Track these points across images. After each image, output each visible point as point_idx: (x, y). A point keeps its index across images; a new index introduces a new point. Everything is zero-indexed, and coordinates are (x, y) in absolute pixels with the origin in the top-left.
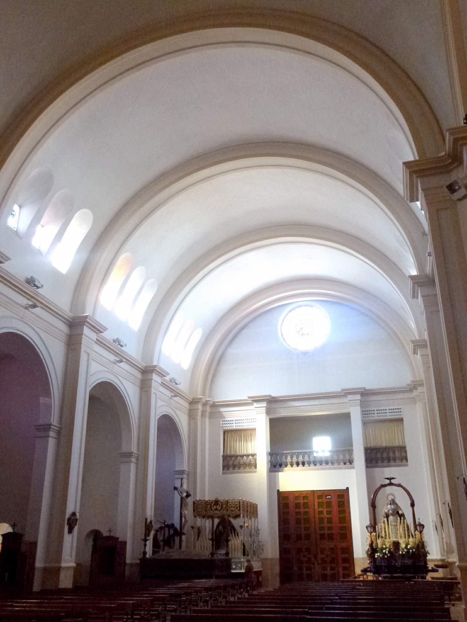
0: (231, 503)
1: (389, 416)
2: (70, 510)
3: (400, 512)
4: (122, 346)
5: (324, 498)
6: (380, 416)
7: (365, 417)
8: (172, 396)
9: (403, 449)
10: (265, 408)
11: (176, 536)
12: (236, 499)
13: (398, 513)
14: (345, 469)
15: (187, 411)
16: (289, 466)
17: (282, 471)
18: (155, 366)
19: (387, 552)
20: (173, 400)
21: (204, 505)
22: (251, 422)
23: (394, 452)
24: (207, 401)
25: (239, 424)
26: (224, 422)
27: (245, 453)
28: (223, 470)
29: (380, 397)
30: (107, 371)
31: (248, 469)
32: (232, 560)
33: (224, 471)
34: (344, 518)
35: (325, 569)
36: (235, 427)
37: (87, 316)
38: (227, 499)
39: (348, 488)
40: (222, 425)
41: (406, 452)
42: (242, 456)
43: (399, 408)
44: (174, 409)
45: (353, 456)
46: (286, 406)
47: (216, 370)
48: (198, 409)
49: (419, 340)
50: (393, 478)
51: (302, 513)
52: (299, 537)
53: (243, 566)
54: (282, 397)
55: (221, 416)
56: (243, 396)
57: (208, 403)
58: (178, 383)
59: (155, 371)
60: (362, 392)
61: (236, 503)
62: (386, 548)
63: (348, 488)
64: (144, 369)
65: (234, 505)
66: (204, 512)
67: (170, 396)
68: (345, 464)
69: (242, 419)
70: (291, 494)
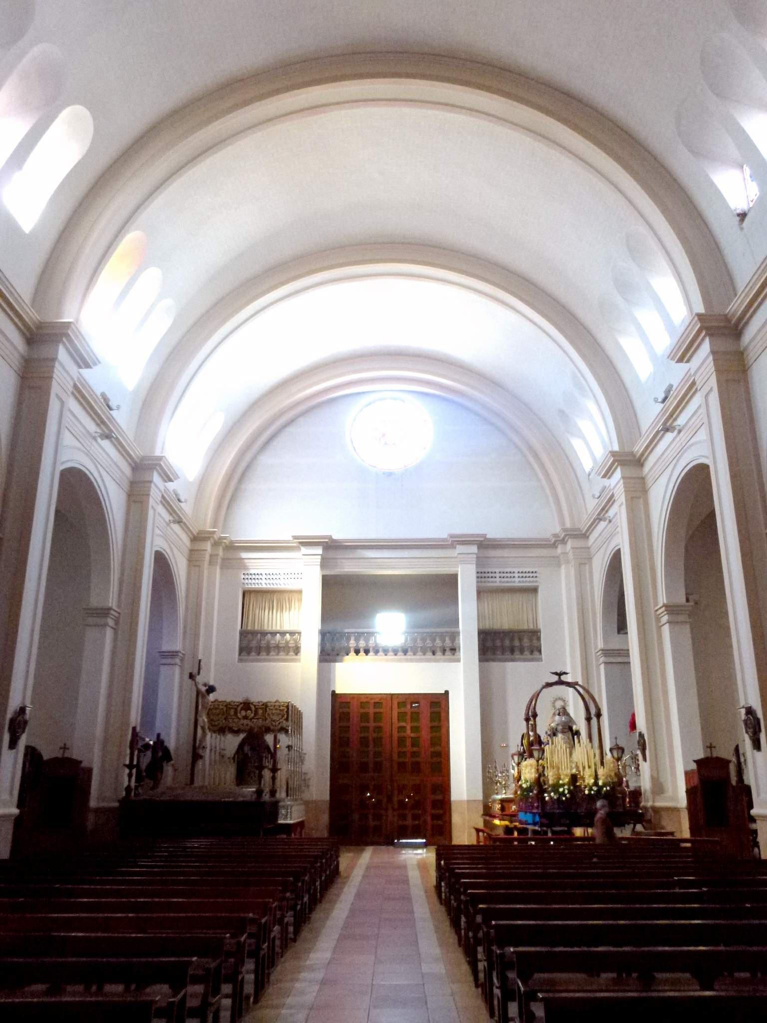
1: (517, 582)
2: (14, 703)
3: (574, 728)
4: (111, 409)
5: (409, 707)
6: (504, 582)
7: (481, 582)
8: (170, 521)
9: (535, 634)
11: (165, 762)
12: (281, 700)
13: (571, 729)
14: (445, 661)
15: (186, 551)
16: (352, 653)
17: (341, 661)
18: (160, 458)
19: (566, 792)
20: (172, 529)
22: (296, 578)
23: (520, 640)
24: (221, 538)
25: (272, 581)
26: (247, 576)
27: (278, 628)
28: (240, 654)
29: (505, 553)
30: (79, 449)
31: (282, 655)
32: (281, 804)
33: (242, 657)
34: (440, 738)
35: (403, 817)
36: (264, 586)
37: (69, 323)
38: (265, 701)
39: (447, 693)
40: (243, 581)
41: (539, 639)
42: (274, 634)
43: (534, 571)
44: (170, 542)
45: (457, 642)
46: (351, 556)
47: (237, 489)
48: (206, 550)
49: (619, 452)
50: (565, 673)
51: (371, 729)
52: (364, 767)
53: (289, 814)
55: (241, 565)
56: (285, 535)
57: (221, 543)
58: (183, 500)
59: (158, 468)
60: (482, 541)
61: (282, 708)
62: (563, 785)
63: (447, 693)
64: (138, 461)
65: (278, 711)
66: (224, 721)
67: (167, 520)
68: (434, 653)
70: (353, 698)
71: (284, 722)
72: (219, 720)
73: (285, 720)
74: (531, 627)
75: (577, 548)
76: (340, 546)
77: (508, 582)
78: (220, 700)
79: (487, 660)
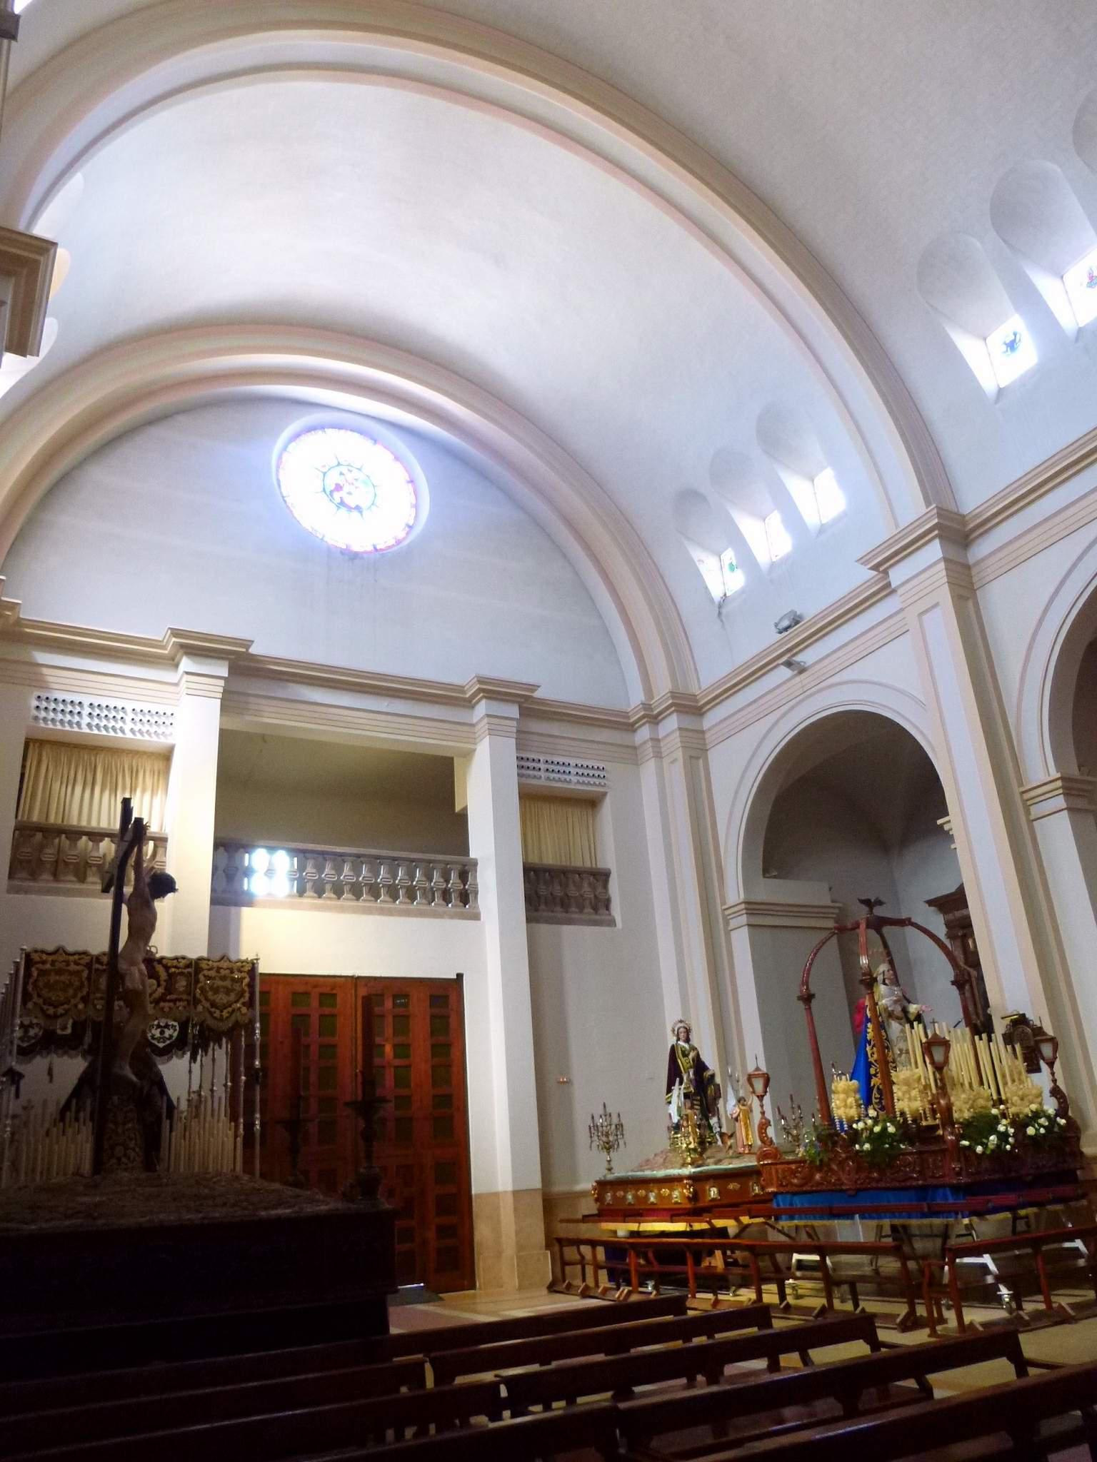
0: (212, 973)
10: (222, 683)
21: (78, 973)
29: (554, 729)
39: (460, 976)
40: (35, 713)
46: (280, 694)
47: (31, 522)
54: (289, 663)
55: (34, 678)
63: (460, 976)
65: (228, 983)
66: (81, 1006)
69: (112, 706)
71: (244, 1010)
72: (68, 1002)
73: (244, 1004)
74: (588, 864)
75: (687, 730)
76: (258, 670)
77: (560, 780)
78: (70, 949)
79: (537, 921)
